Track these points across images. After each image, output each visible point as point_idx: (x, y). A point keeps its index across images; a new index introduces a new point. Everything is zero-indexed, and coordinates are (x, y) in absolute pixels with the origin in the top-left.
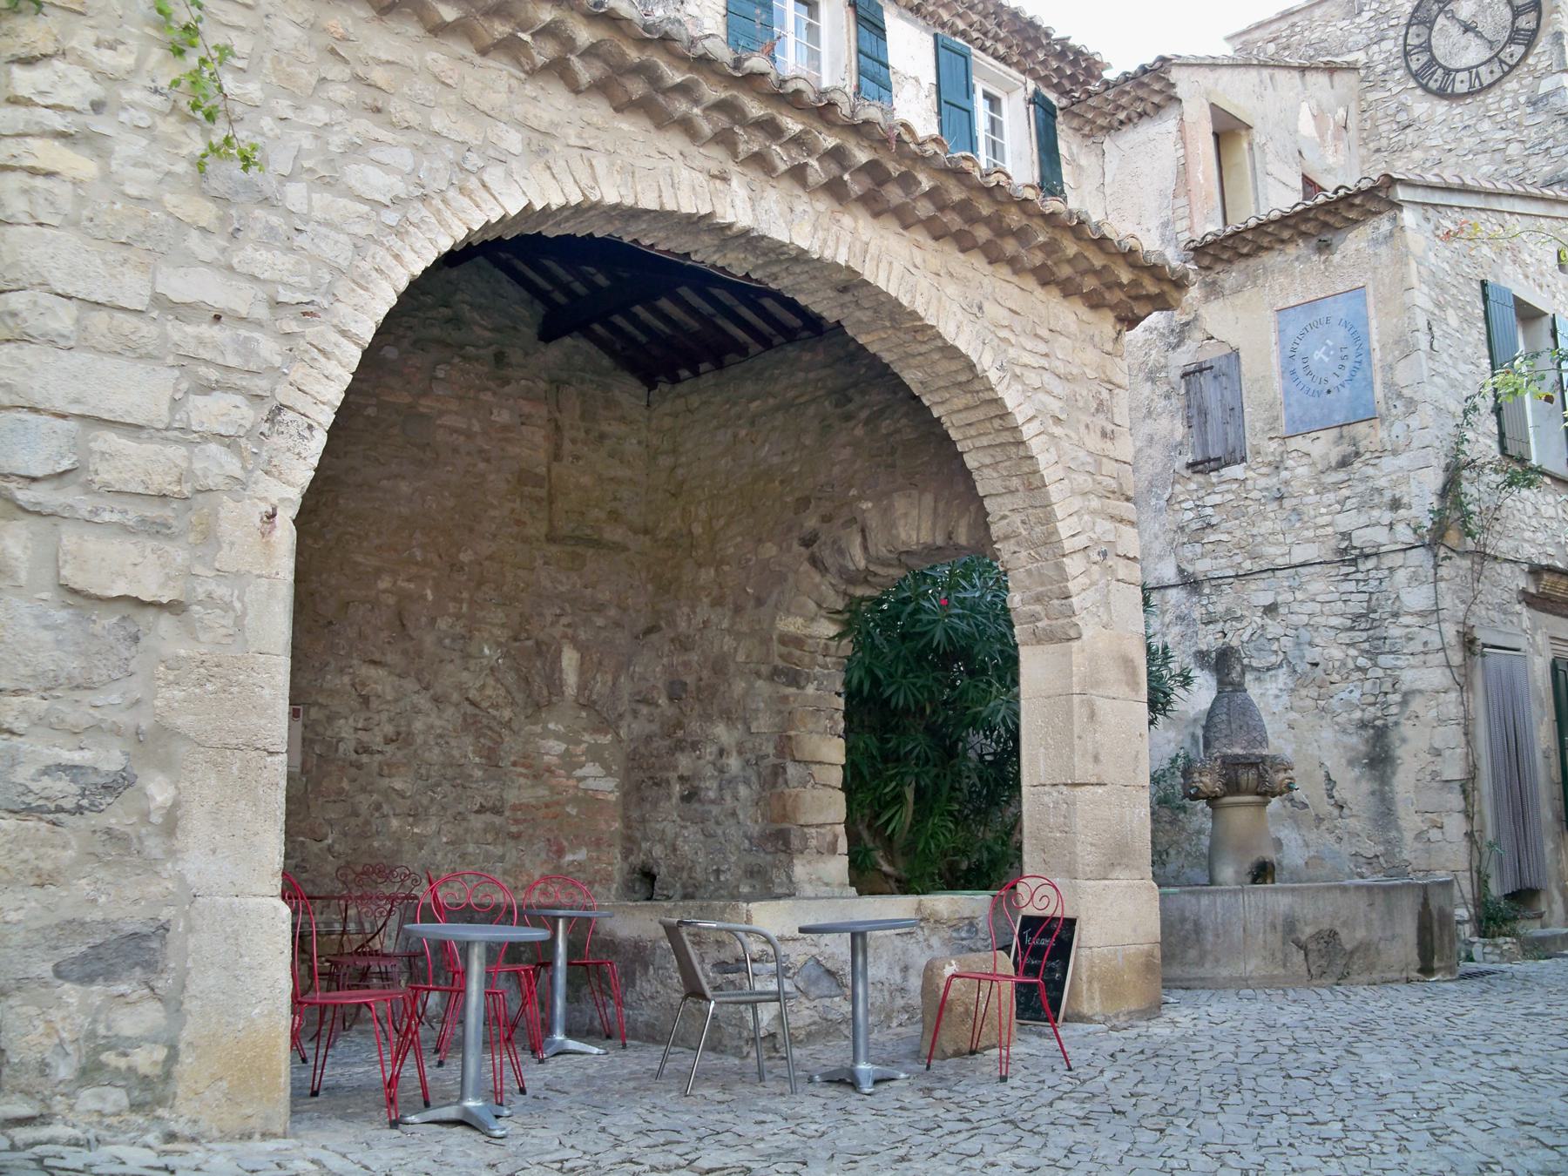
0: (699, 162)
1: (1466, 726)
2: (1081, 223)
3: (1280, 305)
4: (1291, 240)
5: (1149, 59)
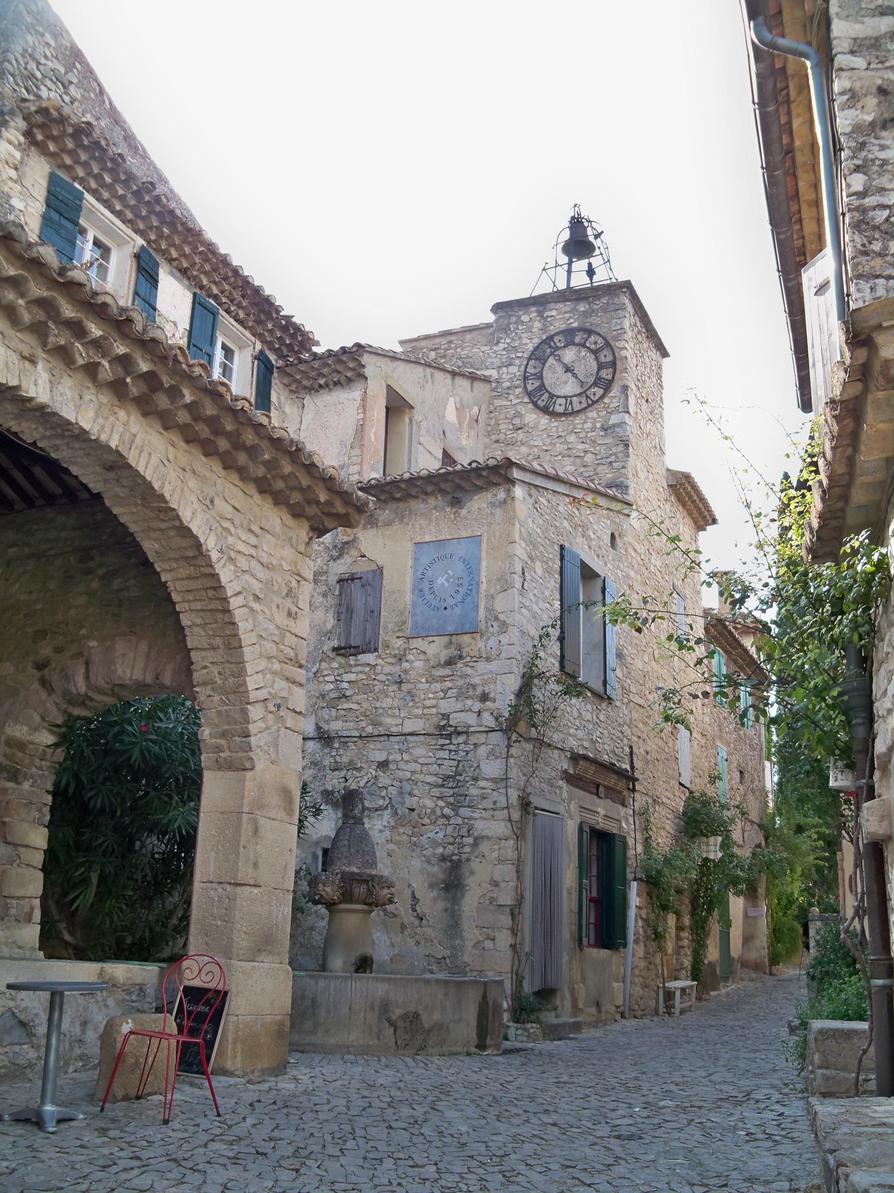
0: (15, 343)
1: (518, 866)
2: (299, 450)
3: (418, 540)
4: (432, 494)
5: (349, 344)
